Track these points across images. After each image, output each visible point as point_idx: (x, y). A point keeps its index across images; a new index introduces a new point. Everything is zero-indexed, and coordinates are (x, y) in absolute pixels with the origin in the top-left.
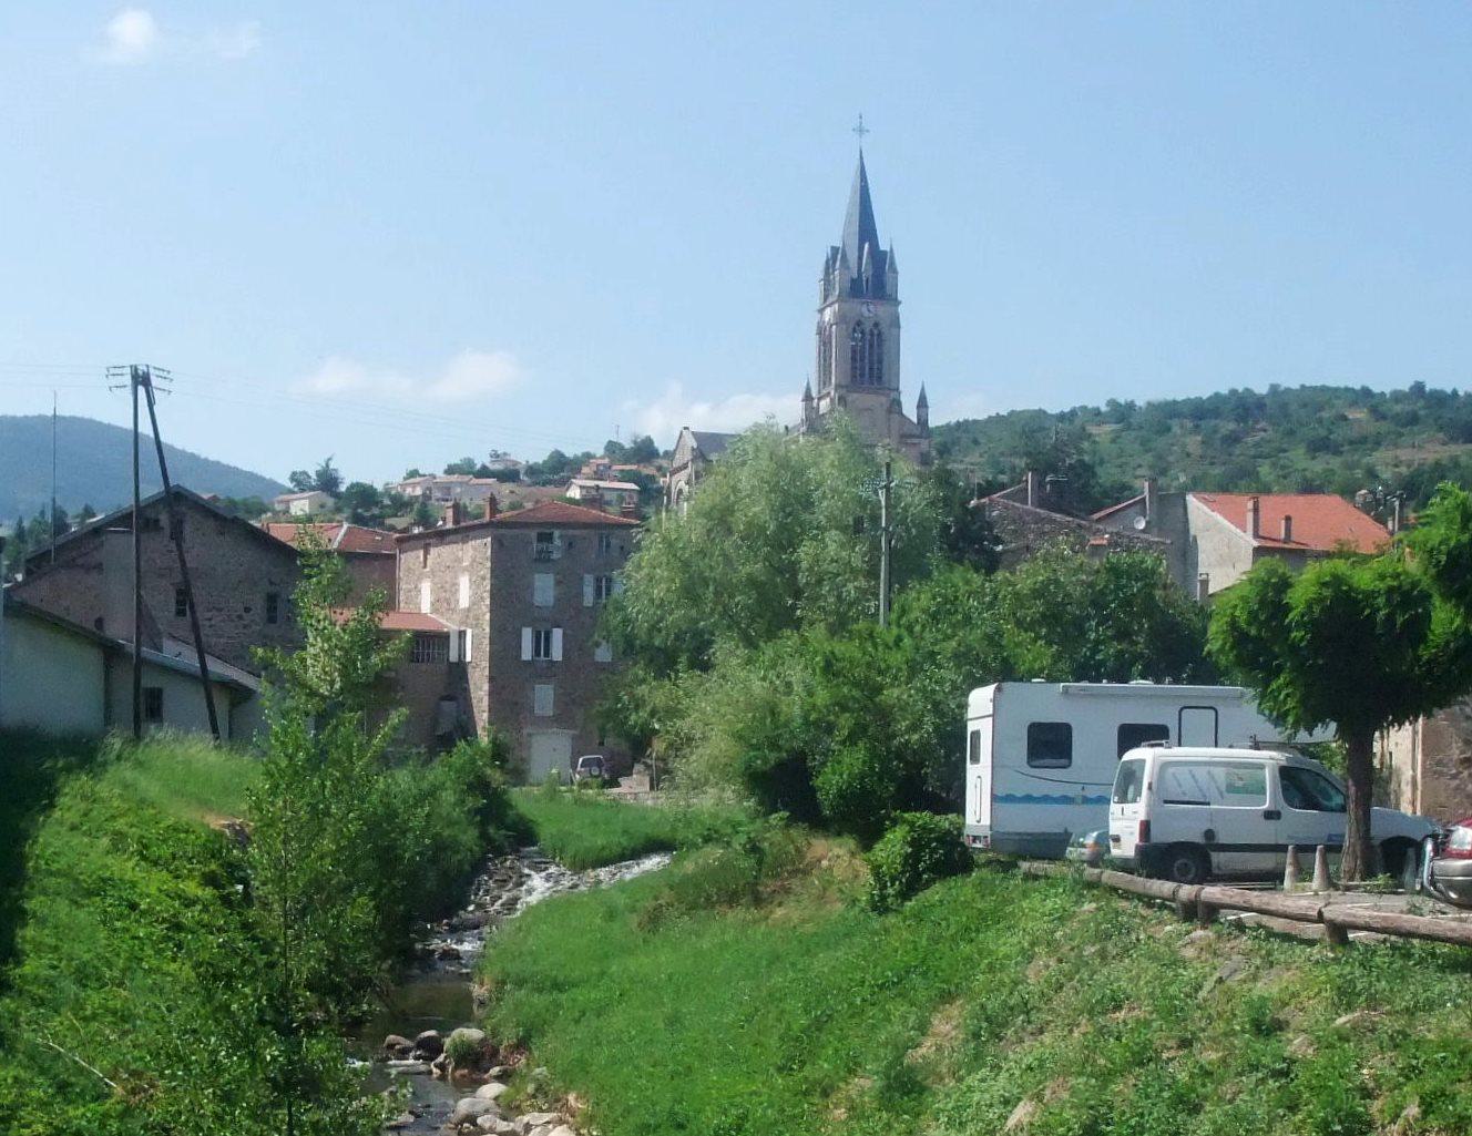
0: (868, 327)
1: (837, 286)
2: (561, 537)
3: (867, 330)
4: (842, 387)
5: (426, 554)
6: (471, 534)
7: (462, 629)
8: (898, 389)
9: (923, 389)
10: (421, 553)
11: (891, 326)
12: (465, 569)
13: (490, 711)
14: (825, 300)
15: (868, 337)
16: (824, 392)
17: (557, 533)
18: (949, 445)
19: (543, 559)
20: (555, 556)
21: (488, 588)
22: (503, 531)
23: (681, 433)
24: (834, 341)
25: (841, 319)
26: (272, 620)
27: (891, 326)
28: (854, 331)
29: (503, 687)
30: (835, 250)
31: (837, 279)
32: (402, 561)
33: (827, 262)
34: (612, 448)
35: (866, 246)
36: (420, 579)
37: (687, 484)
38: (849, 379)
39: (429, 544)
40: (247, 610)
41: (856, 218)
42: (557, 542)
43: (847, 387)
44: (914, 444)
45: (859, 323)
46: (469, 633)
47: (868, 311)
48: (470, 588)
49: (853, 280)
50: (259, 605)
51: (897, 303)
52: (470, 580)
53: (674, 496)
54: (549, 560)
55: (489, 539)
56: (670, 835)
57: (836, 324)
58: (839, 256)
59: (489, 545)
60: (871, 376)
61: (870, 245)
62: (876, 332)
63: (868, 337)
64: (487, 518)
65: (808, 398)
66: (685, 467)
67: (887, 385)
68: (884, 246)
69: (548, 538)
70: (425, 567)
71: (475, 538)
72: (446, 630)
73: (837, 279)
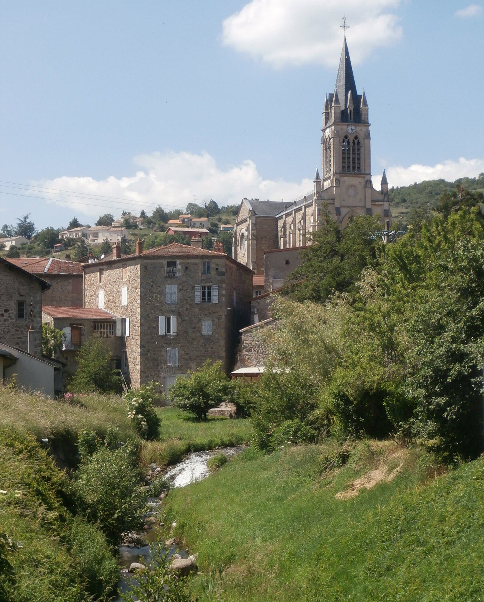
0: (351, 138)
1: (333, 116)
2: (180, 264)
3: (351, 141)
5: (101, 274)
6: (128, 263)
7: (123, 317)
8: (370, 174)
10: (98, 274)
11: (364, 139)
12: (125, 283)
13: (141, 365)
14: (326, 123)
15: (351, 144)
16: (326, 176)
17: (178, 262)
19: (171, 276)
20: (177, 275)
21: (139, 293)
22: (147, 261)
23: (243, 201)
24: (332, 147)
25: (336, 134)
26: (21, 316)
27: (364, 139)
28: (344, 141)
29: (148, 351)
30: (331, 95)
31: (333, 112)
32: (87, 279)
33: (327, 102)
34: (192, 207)
35: (350, 92)
36: (97, 289)
37: (246, 230)
38: (341, 169)
39: (103, 269)
40: (6, 311)
42: (179, 267)
44: (381, 205)
45: (346, 137)
46: (128, 320)
47: (350, 129)
48: (128, 294)
50: (13, 306)
51: (367, 124)
52: (128, 290)
53: (239, 237)
55: (139, 265)
57: (333, 138)
58: (334, 99)
59: (139, 269)
60: (354, 168)
61: (352, 92)
62: (356, 142)
63: (351, 144)
64: (137, 254)
65: (317, 181)
66: (245, 220)
67: (363, 172)
68: (359, 92)
69: (174, 264)
70: (100, 282)
71: (130, 265)
72: (113, 318)
73: (333, 112)
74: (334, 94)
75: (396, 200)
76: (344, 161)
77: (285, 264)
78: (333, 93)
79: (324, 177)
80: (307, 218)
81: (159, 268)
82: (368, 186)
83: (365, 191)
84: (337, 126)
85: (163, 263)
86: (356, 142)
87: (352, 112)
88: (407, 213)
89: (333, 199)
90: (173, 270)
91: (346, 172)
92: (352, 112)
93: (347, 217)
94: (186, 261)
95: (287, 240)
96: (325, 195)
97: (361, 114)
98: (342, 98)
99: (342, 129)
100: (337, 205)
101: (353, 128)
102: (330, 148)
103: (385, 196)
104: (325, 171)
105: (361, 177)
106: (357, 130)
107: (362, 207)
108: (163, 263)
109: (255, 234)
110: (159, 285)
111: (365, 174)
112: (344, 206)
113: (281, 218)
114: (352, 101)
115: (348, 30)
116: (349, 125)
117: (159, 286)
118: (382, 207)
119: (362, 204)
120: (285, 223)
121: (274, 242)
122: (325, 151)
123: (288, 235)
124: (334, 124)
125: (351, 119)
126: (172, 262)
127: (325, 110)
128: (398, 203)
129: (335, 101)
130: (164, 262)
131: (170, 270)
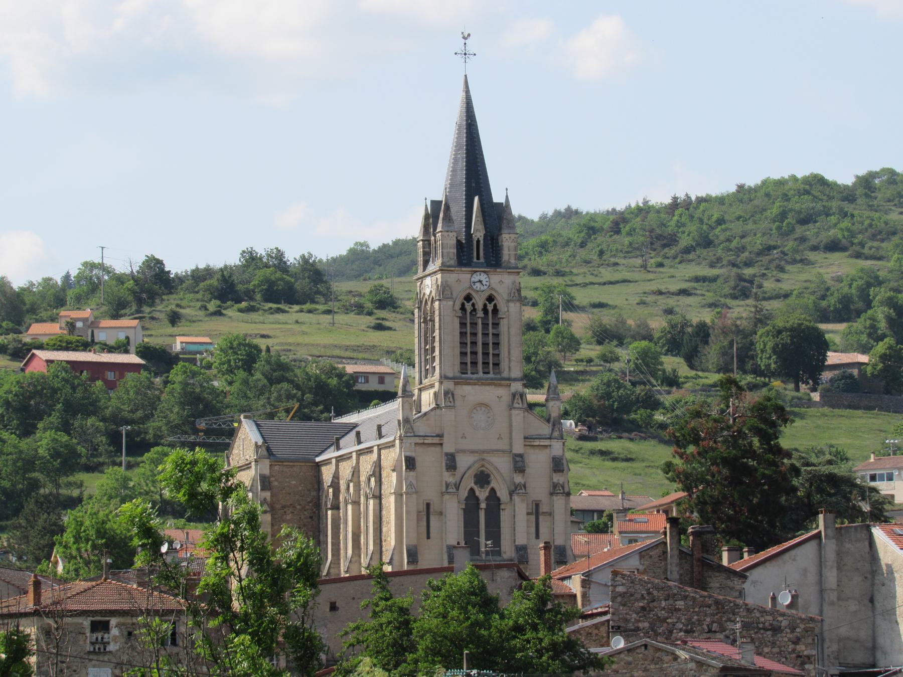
0: (479, 301)
1: (439, 252)
2: (118, 625)
3: (479, 306)
4: (447, 378)
17: (113, 621)
19: (99, 651)
20: (112, 647)
35: (476, 199)
38: (457, 367)
41: (462, 164)
42: (115, 631)
44: (546, 446)
45: (468, 298)
49: (459, 242)
54: (105, 652)
56: (847, 474)
60: (486, 364)
61: (480, 200)
62: (490, 307)
63: (480, 314)
67: (505, 374)
68: (498, 197)
69: (104, 627)
74: (442, 201)
75: (685, 241)
76: (464, 350)
77: (328, 610)
78: (439, 199)
79: (421, 383)
80: (384, 474)
81: (74, 635)
82: (516, 405)
83: (510, 416)
84: (447, 275)
85: (82, 624)
86: (490, 307)
87: (482, 242)
88: (713, 280)
89: (440, 436)
90: (102, 638)
91: (469, 375)
92: (482, 242)
93: (471, 472)
94: (128, 620)
95: (341, 515)
96: (422, 428)
97: (502, 245)
98: (458, 211)
99: (458, 281)
100: (449, 448)
101: (483, 277)
102: (433, 321)
103: (554, 425)
104: (423, 369)
105: (501, 385)
106: (492, 281)
107: (503, 451)
108: (82, 624)
109: (269, 499)
110: (75, 668)
111: (509, 379)
112: (464, 451)
113: (327, 462)
114: (480, 219)
115: (472, 60)
116: (476, 272)
117: (75, 671)
118: (548, 451)
119: (503, 445)
120: (336, 477)
121: (311, 517)
122: (423, 325)
123: (342, 505)
124: (443, 269)
125: (478, 258)
126: (100, 622)
127: (424, 235)
128: (688, 250)
129: (444, 219)
130: (85, 623)
131: (97, 638)
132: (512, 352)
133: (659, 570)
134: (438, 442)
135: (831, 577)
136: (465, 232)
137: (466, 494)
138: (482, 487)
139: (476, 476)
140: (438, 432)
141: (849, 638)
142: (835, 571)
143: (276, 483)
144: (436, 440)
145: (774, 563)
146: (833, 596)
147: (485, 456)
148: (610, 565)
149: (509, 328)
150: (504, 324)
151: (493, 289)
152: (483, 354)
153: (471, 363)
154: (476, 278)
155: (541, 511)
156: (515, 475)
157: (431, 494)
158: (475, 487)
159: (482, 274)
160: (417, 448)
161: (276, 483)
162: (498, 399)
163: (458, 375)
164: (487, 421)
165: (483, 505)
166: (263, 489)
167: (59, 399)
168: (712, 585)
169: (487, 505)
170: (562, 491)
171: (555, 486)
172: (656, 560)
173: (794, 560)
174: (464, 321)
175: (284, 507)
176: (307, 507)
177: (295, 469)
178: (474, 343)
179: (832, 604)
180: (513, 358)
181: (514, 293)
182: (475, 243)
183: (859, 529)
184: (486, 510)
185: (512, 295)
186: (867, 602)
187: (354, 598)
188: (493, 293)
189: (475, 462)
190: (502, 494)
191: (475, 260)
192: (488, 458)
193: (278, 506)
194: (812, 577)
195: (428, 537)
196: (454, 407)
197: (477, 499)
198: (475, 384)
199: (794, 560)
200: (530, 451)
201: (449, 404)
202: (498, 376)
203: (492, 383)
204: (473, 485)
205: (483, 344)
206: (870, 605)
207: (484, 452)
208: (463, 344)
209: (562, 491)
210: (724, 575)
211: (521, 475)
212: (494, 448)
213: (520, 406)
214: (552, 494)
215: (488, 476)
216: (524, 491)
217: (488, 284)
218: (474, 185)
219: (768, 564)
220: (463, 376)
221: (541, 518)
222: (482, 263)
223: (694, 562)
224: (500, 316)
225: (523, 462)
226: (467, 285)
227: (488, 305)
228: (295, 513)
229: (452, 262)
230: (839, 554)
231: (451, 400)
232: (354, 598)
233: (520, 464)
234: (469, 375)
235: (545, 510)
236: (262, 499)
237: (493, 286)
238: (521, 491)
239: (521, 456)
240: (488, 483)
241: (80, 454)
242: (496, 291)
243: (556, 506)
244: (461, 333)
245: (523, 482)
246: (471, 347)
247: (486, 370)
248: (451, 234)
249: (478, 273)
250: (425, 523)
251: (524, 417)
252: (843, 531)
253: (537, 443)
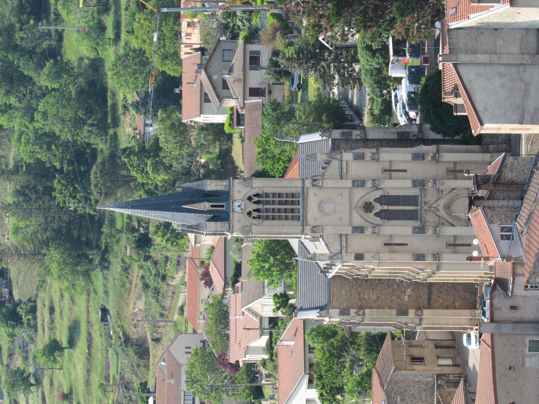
3: (255, 206)
4: (303, 230)
9: (51, 298)
18: (106, 272)
38: (295, 222)
43: (303, 225)
44: (347, 164)
45: (249, 214)
60: (292, 203)
62: (256, 199)
63: (260, 206)
67: (300, 190)
76: (284, 217)
84: (235, 229)
86: (256, 199)
87: (212, 204)
89: (341, 236)
92: (212, 204)
99: (239, 221)
100: (349, 230)
101: (236, 204)
103: (333, 158)
105: (307, 193)
106: (238, 198)
107: (350, 193)
109: (355, 310)
111: (303, 188)
112: (351, 220)
116: (233, 209)
118: (349, 162)
119: (346, 193)
125: (223, 206)
132: (285, 185)
133: (500, 211)
134: (345, 238)
135: (482, 58)
136: (205, 214)
137: (378, 218)
138: (373, 208)
139: (366, 212)
140: (338, 237)
141: (521, 46)
142: (478, 56)
143: (344, 304)
144: (344, 239)
145: (472, 95)
146: (495, 57)
147: (353, 205)
148: (497, 242)
149: (269, 187)
150: (266, 190)
151: (244, 198)
152: (286, 204)
153: (292, 213)
154: (237, 209)
155: (389, 168)
156: (366, 187)
157: (377, 243)
158: (374, 212)
159: (234, 205)
160: (349, 251)
161: (344, 304)
162: (316, 196)
163: (300, 223)
164: (330, 203)
165: (386, 207)
166: (348, 314)
167: (4, 55)
168: (510, 177)
169: (385, 205)
170: (376, 155)
171: (373, 159)
172: (494, 213)
173: (470, 81)
174: (265, 217)
175: (360, 299)
176: (360, 283)
177: (335, 291)
178: (279, 210)
179: (499, 58)
180: (289, 185)
181: (246, 183)
182: (213, 208)
183: (450, 36)
184: (388, 205)
185: (248, 185)
186: (497, 32)
187: (508, 393)
188: (246, 197)
189: (357, 212)
190: (378, 194)
191: (224, 209)
192: (355, 203)
193: (359, 303)
194: (482, 70)
195: (406, 245)
196: (322, 226)
197: (381, 211)
198: (307, 211)
199: (470, 81)
200: (350, 174)
201: (320, 230)
202: (301, 195)
203: (305, 200)
204: (372, 214)
205: (279, 204)
206: (499, 30)
207: (351, 206)
208: (280, 218)
209: (376, 155)
210: (504, 169)
211: (366, 183)
212: (348, 199)
213: (320, 181)
214: (378, 160)
215: (366, 203)
216: (377, 181)
217: (240, 201)
218: (173, 206)
219: (473, 100)
220: (301, 219)
221: (393, 168)
222: (227, 204)
223: (496, 189)
224: (261, 193)
225: (358, 181)
226: (241, 215)
227: (254, 200)
228: (363, 291)
229: (227, 225)
230: (466, 52)
231: (317, 228)
232: (508, 393)
233: (359, 183)
234: (301, 214)
235: (388, 165)
236: (355, 314)
237: (241, 197)
238: (377, 183)
239: (354, 182)
240: (371, 203)
241: (49, 45)
242: (245, 195)
243: (386, 159)
244: (273, 219)
245: (371, 182)
246: (282, 213)
247: (297, 202)
248: (208, 225)
249: (234, 207)
250: (397, 247)
251: (328, 179)
252: (452, 47)
253: (344, 170)
